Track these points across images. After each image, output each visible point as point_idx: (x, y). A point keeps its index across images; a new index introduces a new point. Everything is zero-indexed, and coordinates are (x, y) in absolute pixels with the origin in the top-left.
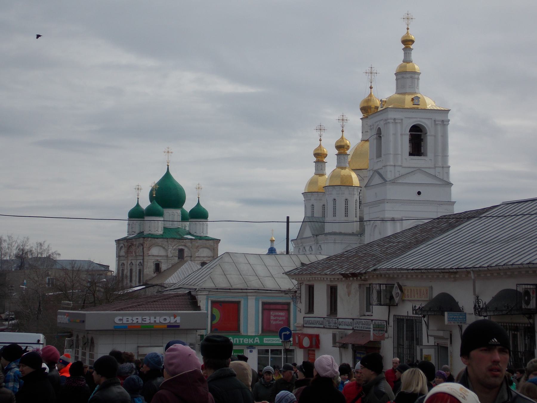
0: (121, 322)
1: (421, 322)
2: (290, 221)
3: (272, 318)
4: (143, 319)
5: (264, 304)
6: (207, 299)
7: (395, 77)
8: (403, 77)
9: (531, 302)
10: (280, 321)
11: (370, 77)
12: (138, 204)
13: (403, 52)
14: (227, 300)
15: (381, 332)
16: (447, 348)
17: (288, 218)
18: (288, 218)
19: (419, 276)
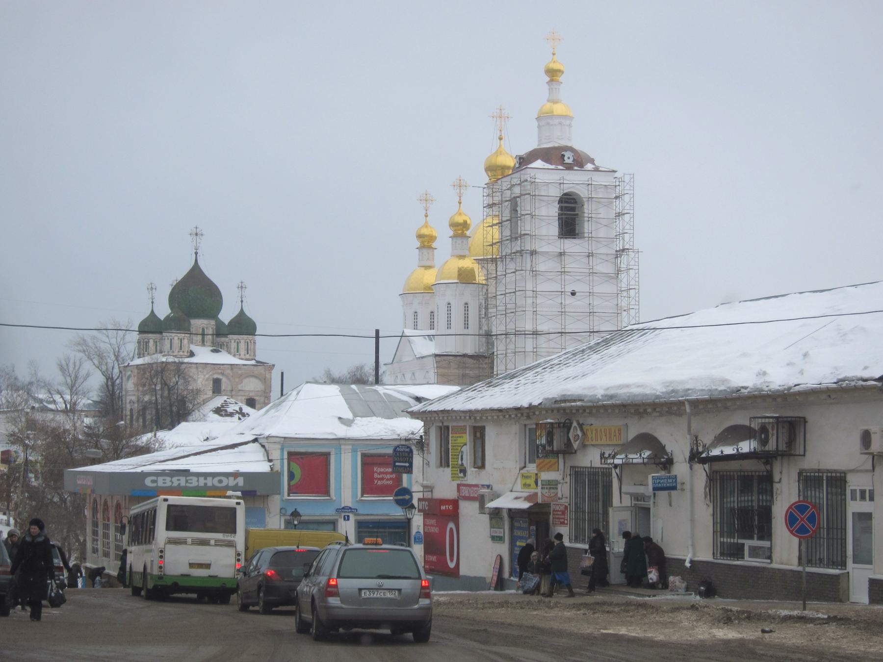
0: (155, 485)
1: (610, 475)
2: (380, 335)
3: (376, 476)
4: (187, 481)
5: (364, 456)
6: (282, 449)
7: (536, 124)
8: (548, 124)
9: (770, 442)
10: (388, 480)
11: (498, 123)
12: (152, 311)
13: (547, 87)
14: (310, 450)
15: (552, 491)
16: (649, 509)
17: (377, 332)
18: (377, 332)
19: (610, 411)
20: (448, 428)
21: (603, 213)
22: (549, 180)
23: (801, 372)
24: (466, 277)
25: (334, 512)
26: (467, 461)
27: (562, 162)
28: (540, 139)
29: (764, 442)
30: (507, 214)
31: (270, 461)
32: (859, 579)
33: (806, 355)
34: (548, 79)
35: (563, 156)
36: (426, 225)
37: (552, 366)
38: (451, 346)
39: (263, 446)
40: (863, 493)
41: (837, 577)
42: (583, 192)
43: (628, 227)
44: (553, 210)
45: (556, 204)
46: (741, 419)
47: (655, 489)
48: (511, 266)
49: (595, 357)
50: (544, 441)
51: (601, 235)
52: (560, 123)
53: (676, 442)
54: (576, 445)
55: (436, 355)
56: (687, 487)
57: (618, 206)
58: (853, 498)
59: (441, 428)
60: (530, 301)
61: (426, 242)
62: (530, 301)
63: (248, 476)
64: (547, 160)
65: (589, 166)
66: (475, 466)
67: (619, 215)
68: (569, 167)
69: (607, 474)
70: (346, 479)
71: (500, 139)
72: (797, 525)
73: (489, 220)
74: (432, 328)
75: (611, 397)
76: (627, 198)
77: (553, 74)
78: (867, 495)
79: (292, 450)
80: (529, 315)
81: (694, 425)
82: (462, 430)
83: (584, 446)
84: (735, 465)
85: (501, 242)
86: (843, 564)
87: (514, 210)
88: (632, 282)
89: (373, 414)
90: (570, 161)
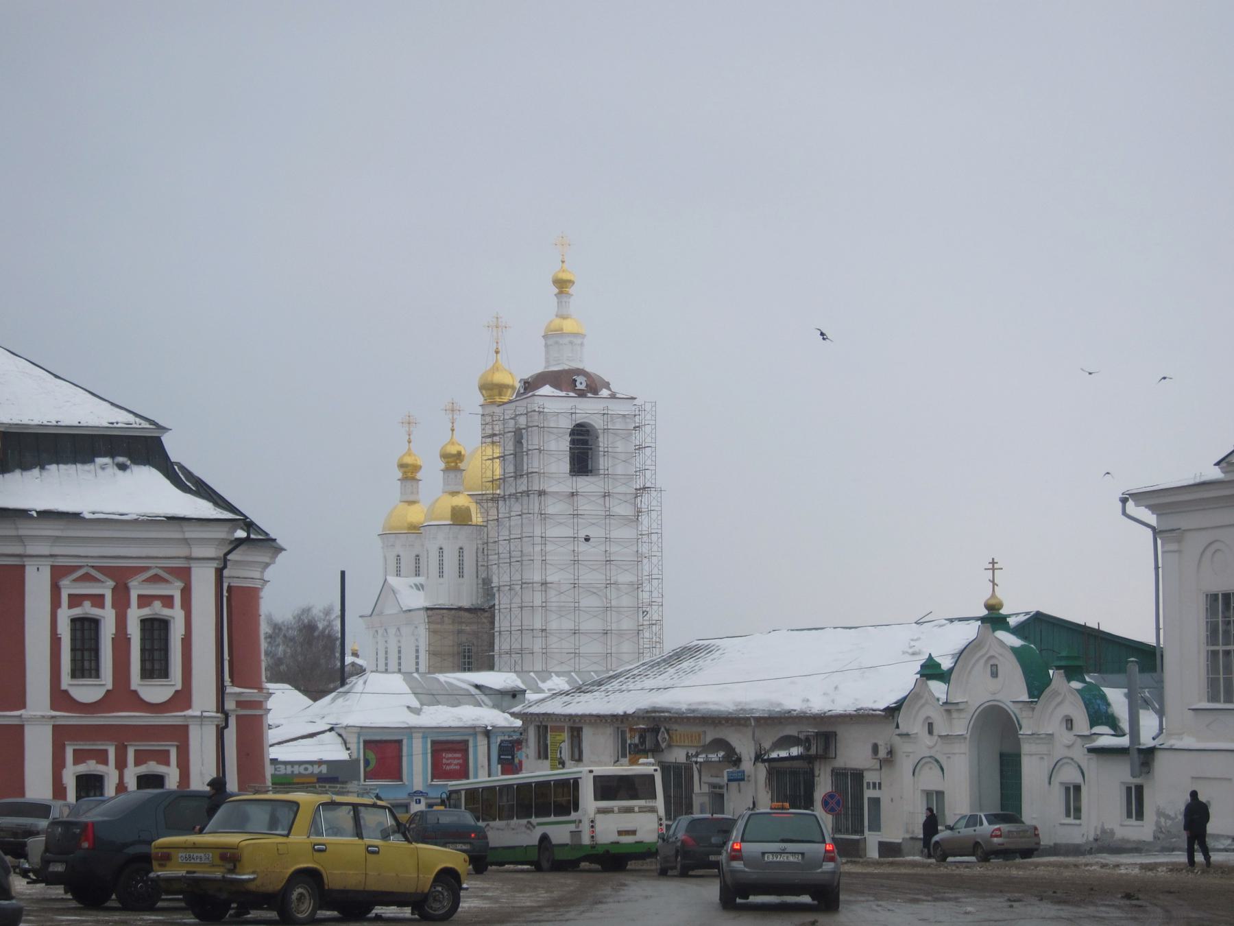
3: (444, 761)
5: (433, 743)
7: (543, 342)
8: (557, 343)
20: (546, 727)
21: (620, 446)
22: (558, 408)
23: (833, 701)
24: (460, 518)
25: (405, 796)
26: (566, 755)
27: (574, 389)
28: (547, 361)
29: (808, 749)
30: (510, 448)
31: (348, 749)
32: (872, 841)
33: (836, 688)
34: (556, 291)
35: (575, 381)
36: (409, 453)
37: (634, 676)
38: (443, 600)
39: (340, 735)
40: (874, 784)
41: (858, 841)
42: (597, 423)
43: (649, 462)
44: (562, 445)
45: (561, 434)
46: (791, 731)
47: (729, 780)
48: (517, 508)
49: (671, 671)
50: (636, 740)
51: (619, 472)
52: (571, 343)
53: (744, 746)
54: (663, 745)
55: (428, 609)
56: (753, 779)
57: (638, 438)
58: (868, 787)
59: (539, 727)
60: (538, 548)
61: (409, 473)
62: (538, 548)
63: (330, 763)
64: (556, 386)
65: (605, 393)
66: (572, 759)
67: (640, 448)
68: (582, 394)
69: (688, 768)
70: (417, 767)
71: (497, 352)
72: (829, 807)
73: (489, 452)
74: (417, 574)
75: (694, 711)
76: (648, 429)
77: (562, 285)
78: (877, 786)
79: (368, 738)
80: (537, 564)
81: (757, 734)
82: (561, 729)
83: (670, 746)
84: (787, 764)
85: (504, 479)
86: (862, 832)
87: (518, 442)
88: (654, 525)
89: (438, 703)
90: (583, 387)
